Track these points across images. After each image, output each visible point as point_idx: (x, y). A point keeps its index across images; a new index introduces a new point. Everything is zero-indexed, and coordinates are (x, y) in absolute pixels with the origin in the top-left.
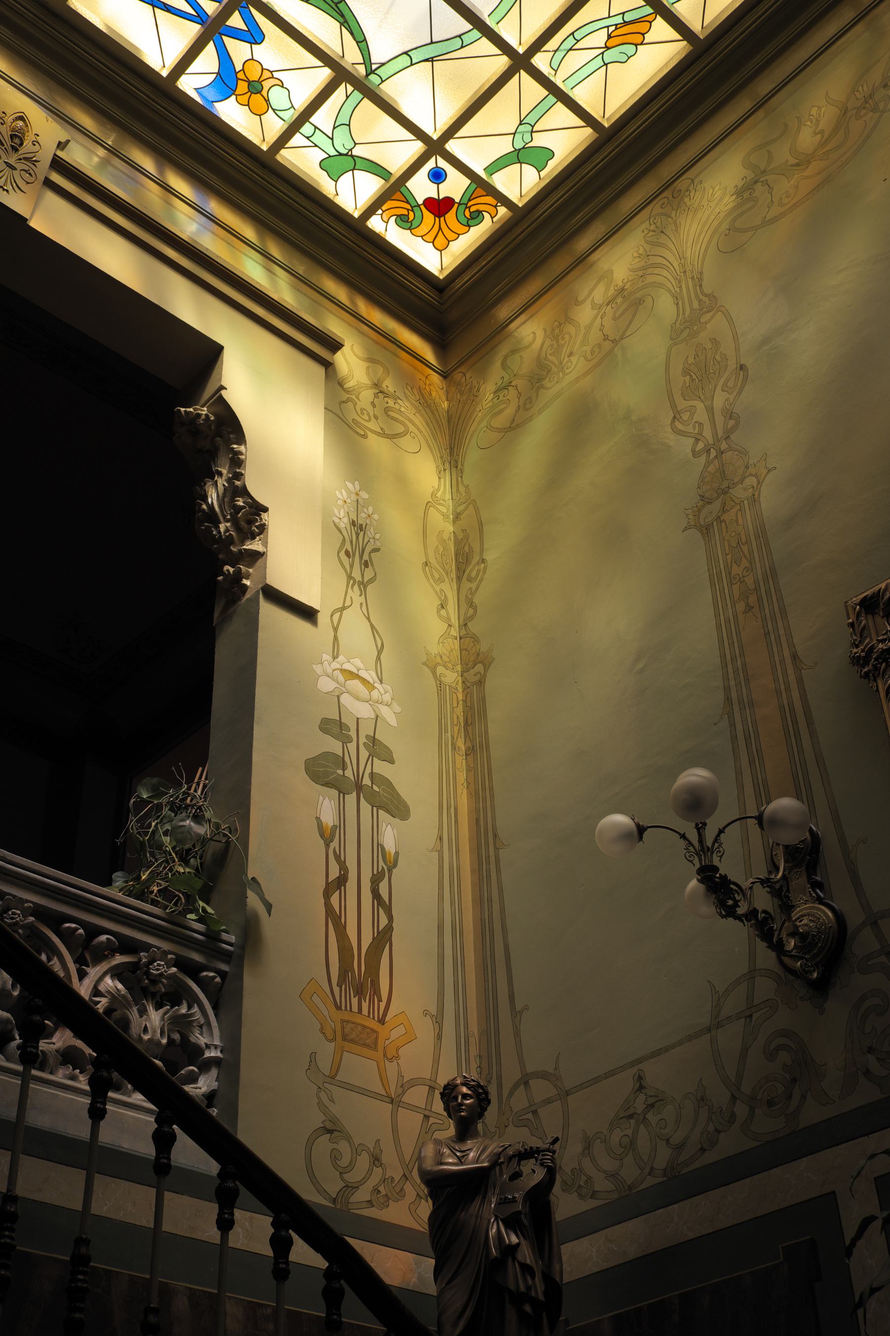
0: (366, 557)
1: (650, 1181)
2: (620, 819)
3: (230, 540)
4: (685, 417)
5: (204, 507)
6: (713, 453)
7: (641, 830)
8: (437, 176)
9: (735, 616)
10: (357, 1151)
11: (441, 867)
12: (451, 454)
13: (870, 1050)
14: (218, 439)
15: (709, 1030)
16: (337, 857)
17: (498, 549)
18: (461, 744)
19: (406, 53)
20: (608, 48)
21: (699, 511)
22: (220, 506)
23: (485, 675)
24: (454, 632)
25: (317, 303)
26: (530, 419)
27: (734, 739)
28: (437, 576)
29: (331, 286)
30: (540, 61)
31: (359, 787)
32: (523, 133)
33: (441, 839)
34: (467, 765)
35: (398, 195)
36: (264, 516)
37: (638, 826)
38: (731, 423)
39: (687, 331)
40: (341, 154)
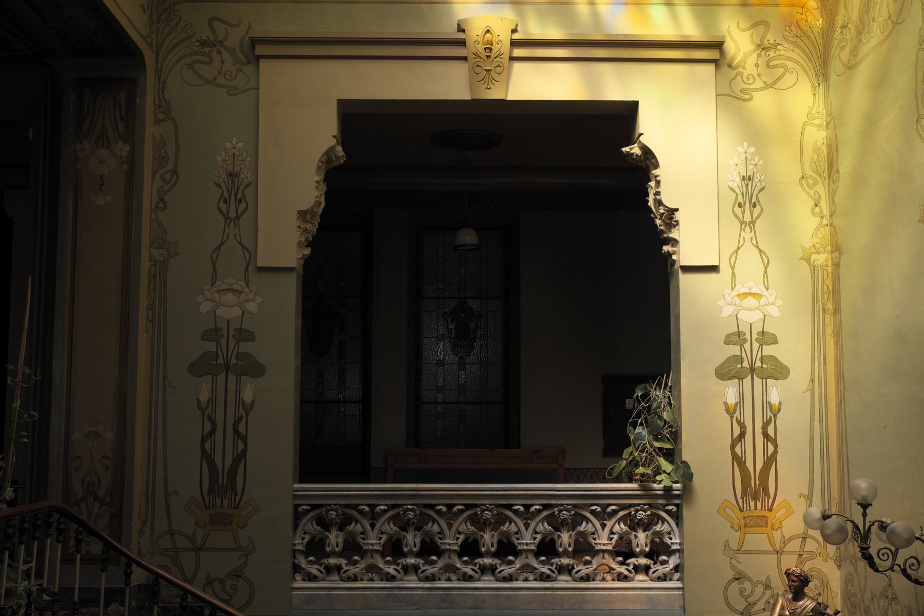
0: (754, 200)
16: (739, 422)
17: (846, 164)
18: (830, 306)
28: (811, 182)
33: (813, 381)
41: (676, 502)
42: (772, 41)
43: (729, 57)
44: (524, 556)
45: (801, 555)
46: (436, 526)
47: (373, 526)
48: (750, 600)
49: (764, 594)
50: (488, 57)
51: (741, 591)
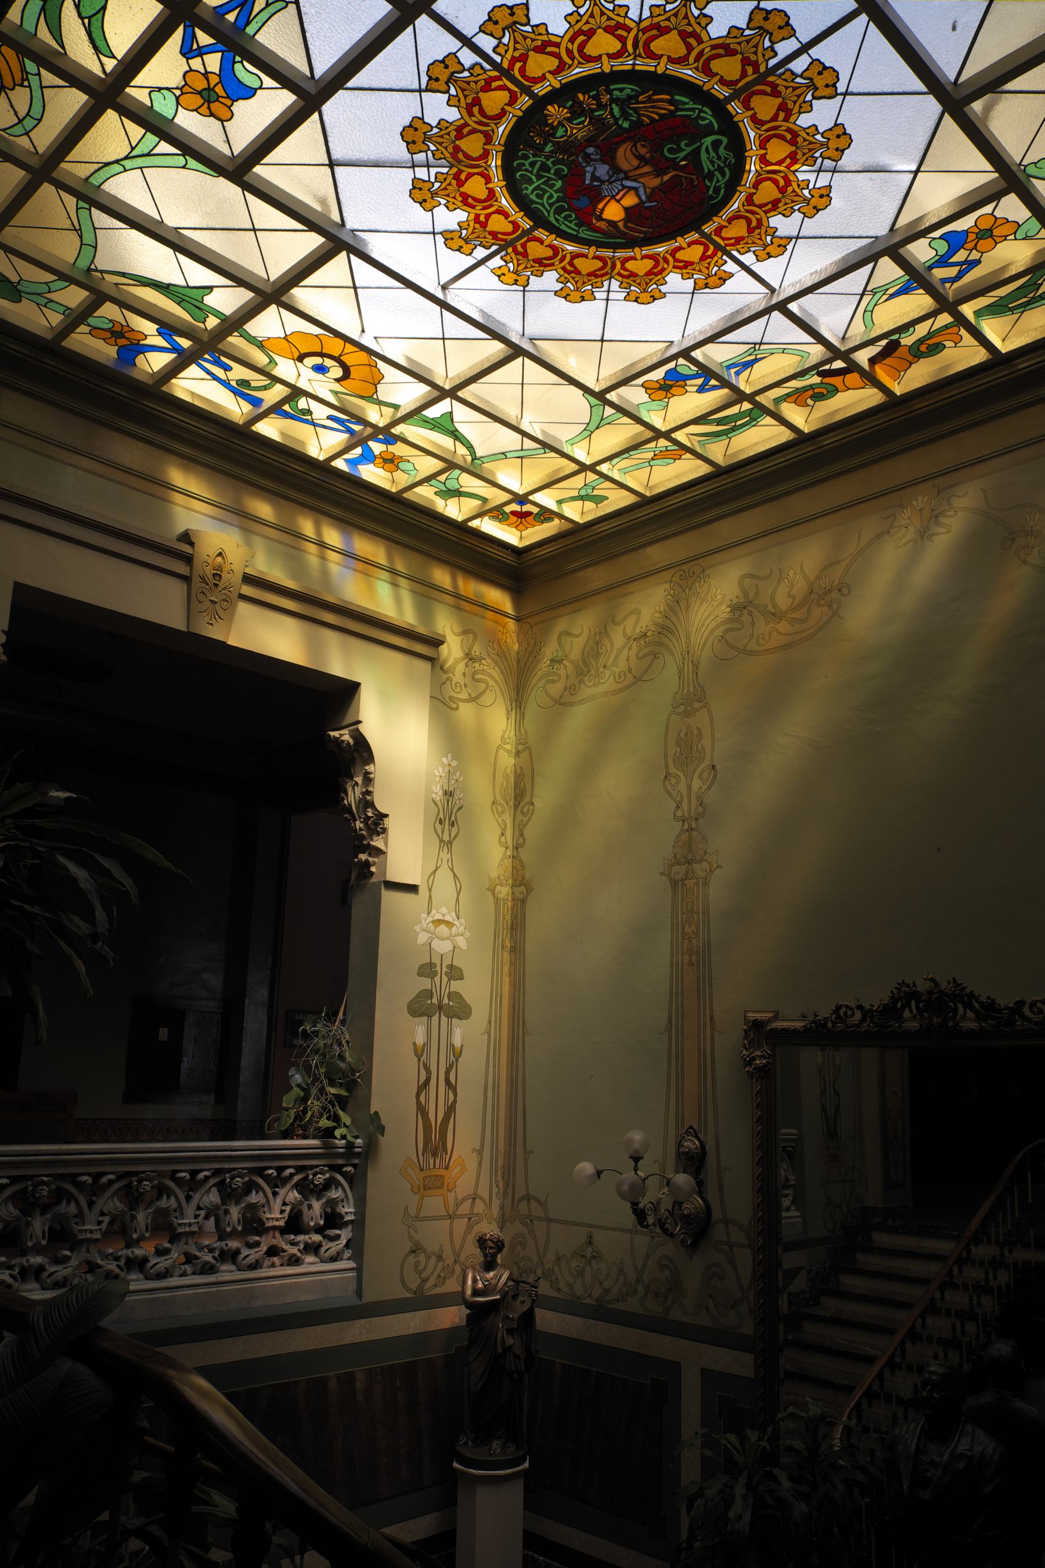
0: (453, 818)
1: (588, 1301)
7: (599, 1174)
10: (428, 1258)
12: (517, 694)
13: (711, 1296)
16: (425, 1066)
17: (545, 798)
18: (508, 944)
23: (526, 897)
25: (429, 597)
26: (572, 704)
28: (500, 809)
31: (440, 1007)
33: (490, 1022)
36: (386, 820)
38: (701, 809)
41: (355, 1165)
42: (478, 653)
43: (442, 659)
44: (183, 1241)
45: (470, 1219)
46: (73, 1206)
47: (91, 1204)
48: (423, 1276)
49: (436, 1266)
50: (216, 585)
51: (416, 1265)
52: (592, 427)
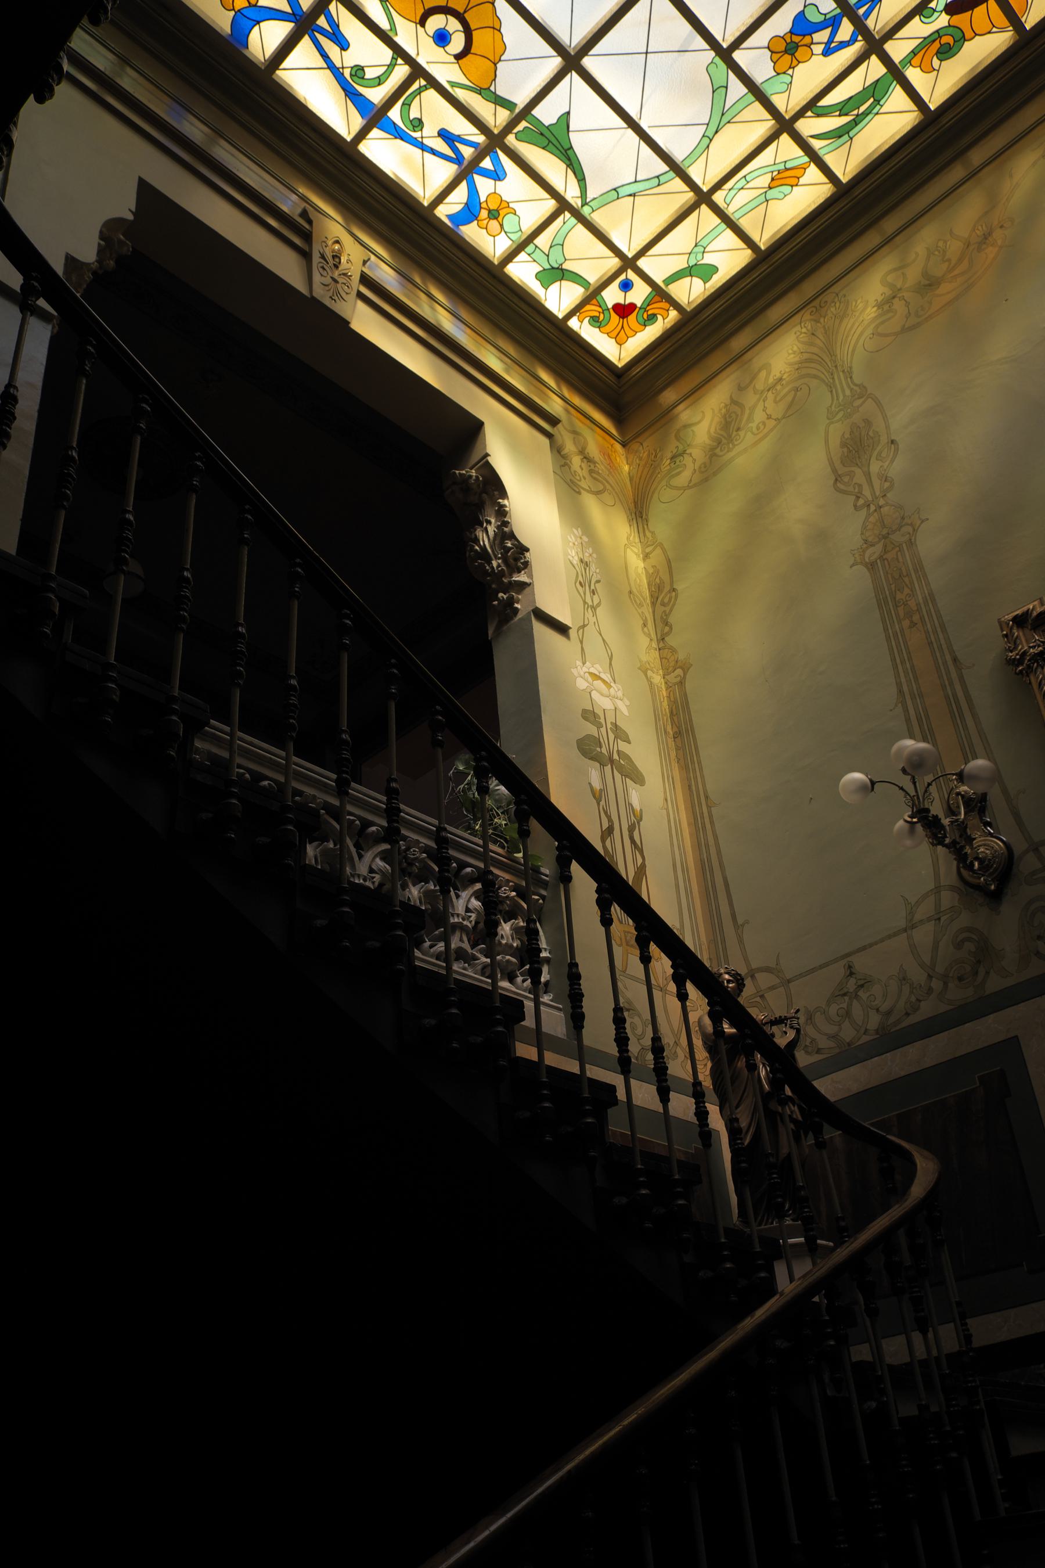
0: (593, 587)
1: (865, 1039)
2: (857, 775)
3: (502, 574)
4: (846, 479)
5: (477, 548)
6: (873, 508)
8: (626, 286)
9: (902, 630)
11: (669, 821)
13: (1039, 938)
14: (484, 495)
15: (905, 930)
16: (606, 813)
19: (615, 189)
20: (770, 188)
21: (864, 551)
22: (491, 547)
24: (654, 645)
27: (908, 720)
29: (544, 375)
30: (718, 197)
31: (612, 761)
32: (697, 253)
34: (676, 745)
35: (594, 301)
36: (527, 554)
37: (871, 780)
38: (887, 485)
39: (841, 414)
40: (553, 268)
52: (710, 134)
